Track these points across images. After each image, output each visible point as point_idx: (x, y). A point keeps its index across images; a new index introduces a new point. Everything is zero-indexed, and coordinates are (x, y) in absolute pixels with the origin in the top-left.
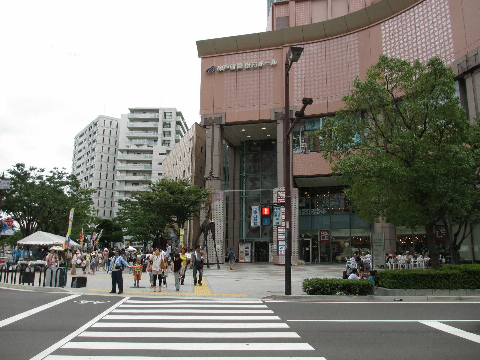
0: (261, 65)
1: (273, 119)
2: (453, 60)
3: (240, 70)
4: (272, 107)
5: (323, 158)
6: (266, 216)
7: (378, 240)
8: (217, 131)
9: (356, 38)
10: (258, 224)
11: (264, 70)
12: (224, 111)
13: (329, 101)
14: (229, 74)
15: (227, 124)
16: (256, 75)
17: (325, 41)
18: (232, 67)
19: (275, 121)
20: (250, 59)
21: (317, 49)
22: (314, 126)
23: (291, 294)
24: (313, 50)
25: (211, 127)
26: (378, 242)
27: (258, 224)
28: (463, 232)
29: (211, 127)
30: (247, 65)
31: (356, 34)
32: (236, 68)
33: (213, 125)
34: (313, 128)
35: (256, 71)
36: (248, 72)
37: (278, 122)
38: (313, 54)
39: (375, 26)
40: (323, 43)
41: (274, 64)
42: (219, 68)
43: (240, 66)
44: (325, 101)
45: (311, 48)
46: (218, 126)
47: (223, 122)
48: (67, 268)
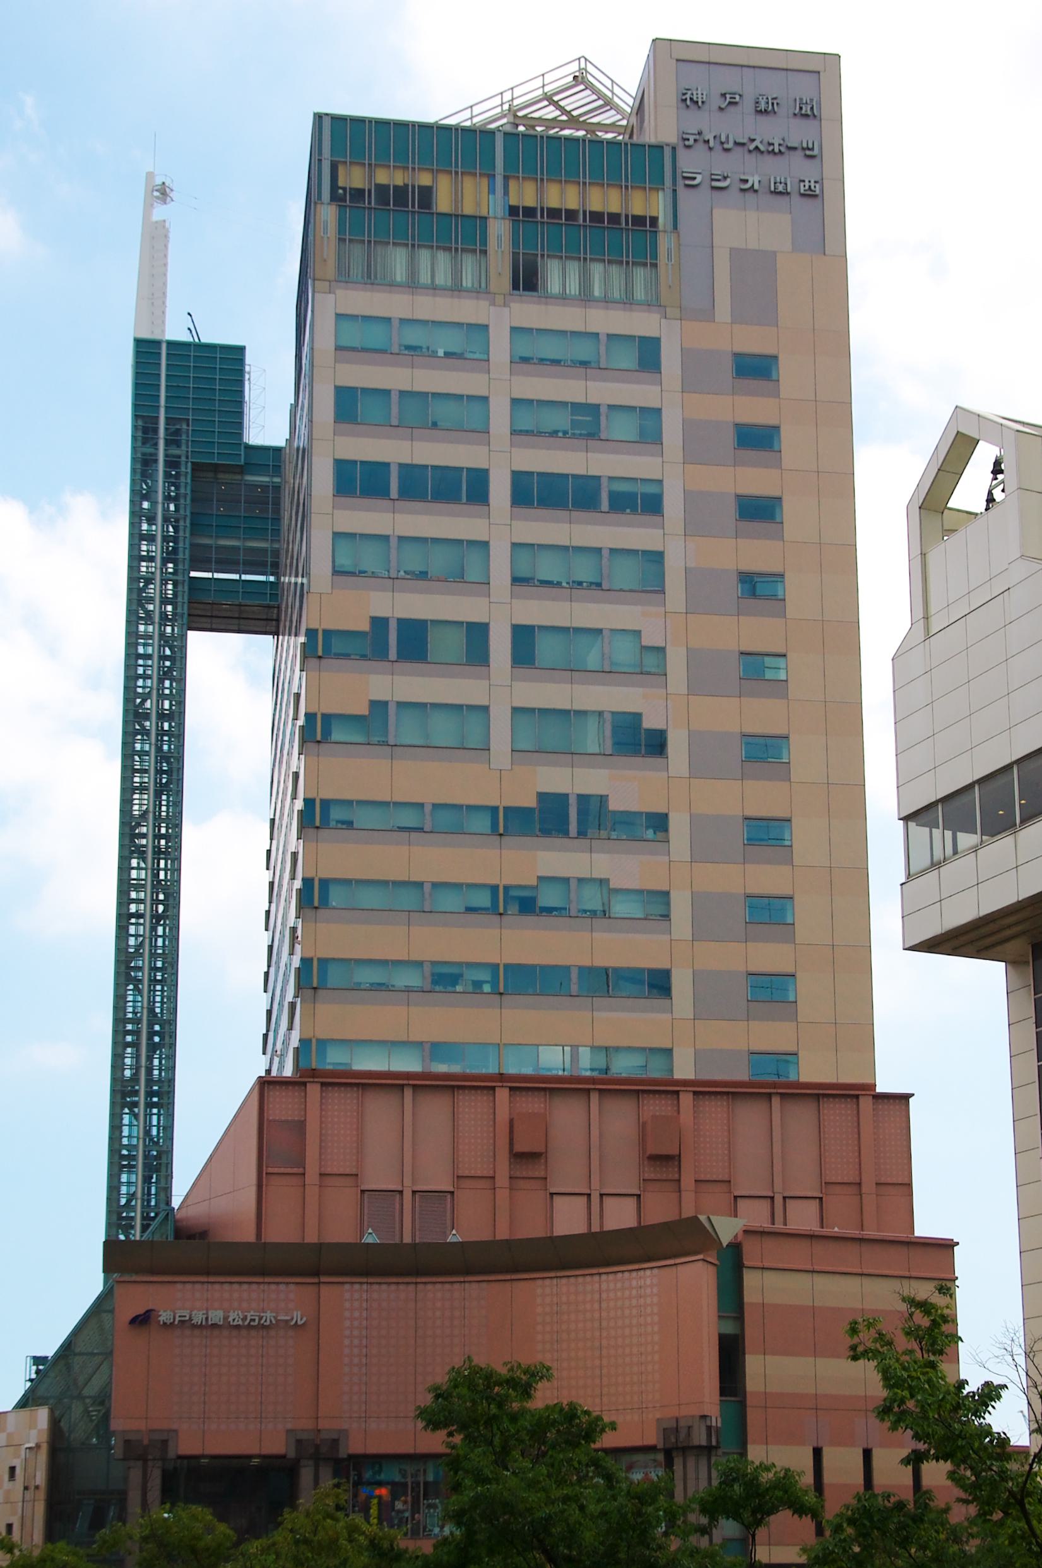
0: (268, 1323)
1: (292, 1454)
3: (214, 1326)
4: (289, 1426)
6: (145, 497)
7: (731, 101)
11: (273, 1333)
12: (174, 1427)
14: (188, 1332)
16: (253, 1342)
17: (600, 1274)
18: (198, 1318)
22: (380, 1472)
23: (231, 361)
25: (140, 1463)
26: (721, 164)
28: (706, 1476)
29: (140, 1463)
32: (207, 1319)
33: (145, 1461)
34: (378, 1478)
35: (253, 1333)
36: (235, 1333)
37: (303, 1462)
40: (412, 1287)
41: (300, 1323)
42: (165, 1316)
43: (216, 1316)
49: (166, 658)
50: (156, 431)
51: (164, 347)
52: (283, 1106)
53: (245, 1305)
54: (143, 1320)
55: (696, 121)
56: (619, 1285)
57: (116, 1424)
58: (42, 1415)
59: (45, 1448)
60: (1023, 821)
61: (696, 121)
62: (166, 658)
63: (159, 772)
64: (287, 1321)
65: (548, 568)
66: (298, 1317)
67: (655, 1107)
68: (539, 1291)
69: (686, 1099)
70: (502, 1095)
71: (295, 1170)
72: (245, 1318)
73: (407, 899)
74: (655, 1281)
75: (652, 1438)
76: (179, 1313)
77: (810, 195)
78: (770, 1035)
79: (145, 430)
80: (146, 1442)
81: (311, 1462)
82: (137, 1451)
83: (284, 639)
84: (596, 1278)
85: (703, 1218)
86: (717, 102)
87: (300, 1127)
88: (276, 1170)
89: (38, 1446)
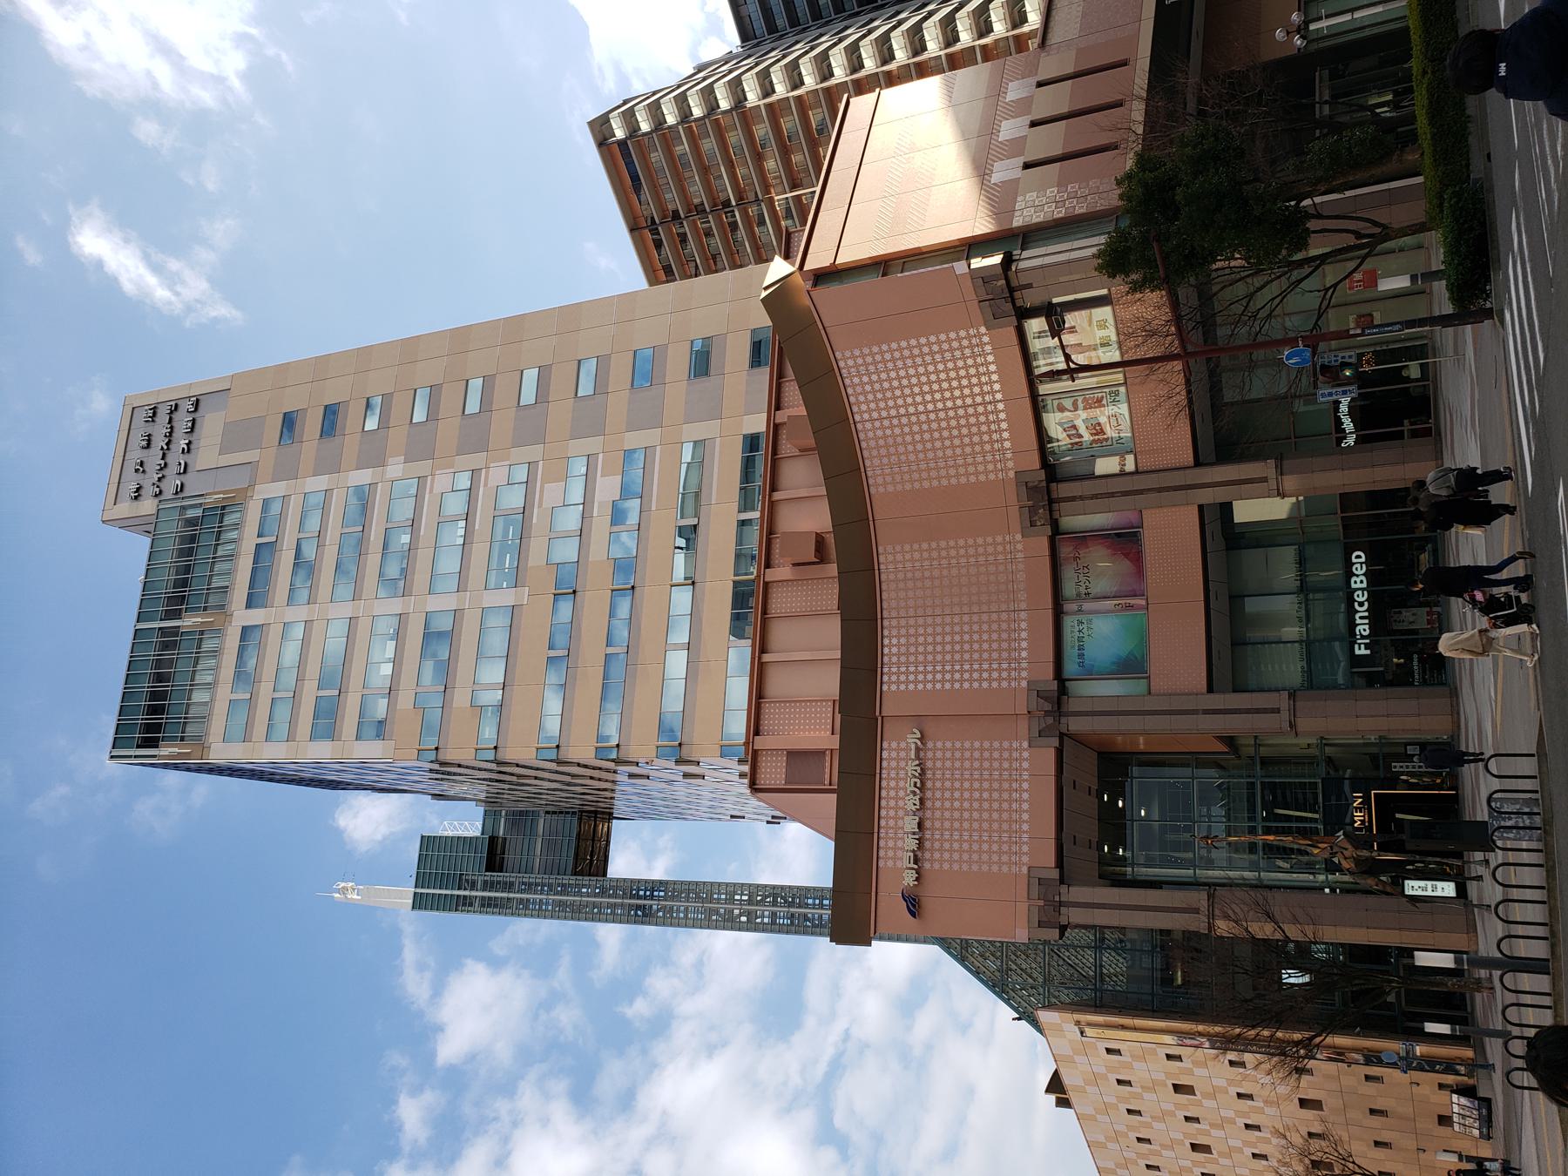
1: (1055, 742)
2: (983, 330)
3: (920, 825)
4: (1025, 745)
5: (1052, 1098)
8: (1077, 893)
9: (848, 354)
10: (1409, 892)
11: (929, 764)
12: (1025, 870)
13: (1023, 606)
15: (1060, 864)
18: (912, 844)
19: (1062, 736)
20: (896, 818)
21: (898, 637)
23: (429, 844)
24: (899, 645)
27: (1409, 892)
30: (911, 803)
31: (838, 355)
33: (1061, 904)
35: (929, 784)
38: (908, 645)
39: (1052, 24)
42: (909, 879)
43: (911, 824)
44: (1023, 615)
45: (895, 650)
46: (1064, 889)
47: (1055, 874)
48: (1217, 1035)
49: (775, 901)
50: (490, 898)
51: (420, 890)
52: (773, 772)
53: (901, 793)
54: (914, 905)
55: (149, 490)
56: (862, 398)
57: (1022, 936)
58: (1044, 1016)
59: (1077, 1016)
60: (1455, 788)
61: (149, 490)
62: (775, 901)
63: (774, 903)
64: (918, 749)
65: (393, 570)
66: (912, 739)
67: (786, 448)
68: (881, 490)
69: (781, 417)
70: (771, 575)
71: (828, 758)
72: (914, 793)
73: (617, 670)
74: (848, 354)
75: (1011, 332)
76: (906, 862)
77: (197, 404)
78: (738, 351)
79: (489, 906)
80: (1041, 903)
81: (1063, 720)
82: (1050, 913)
83: (620, 807)
84: (859, 426)
85: (764, 294)
86: (140, 475)
87: (792, 755)
88: (827, 776)
89: (1078, 1023)
